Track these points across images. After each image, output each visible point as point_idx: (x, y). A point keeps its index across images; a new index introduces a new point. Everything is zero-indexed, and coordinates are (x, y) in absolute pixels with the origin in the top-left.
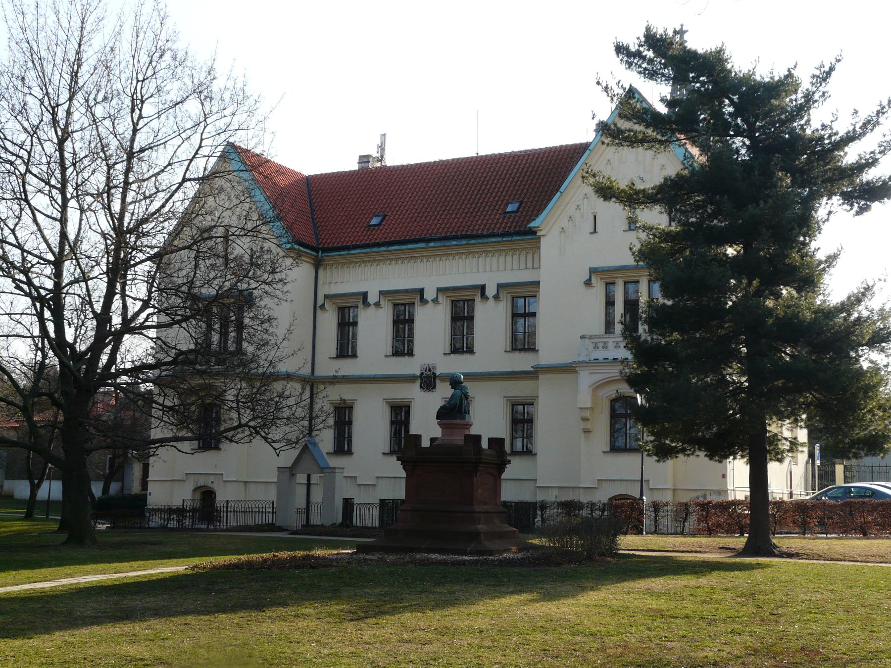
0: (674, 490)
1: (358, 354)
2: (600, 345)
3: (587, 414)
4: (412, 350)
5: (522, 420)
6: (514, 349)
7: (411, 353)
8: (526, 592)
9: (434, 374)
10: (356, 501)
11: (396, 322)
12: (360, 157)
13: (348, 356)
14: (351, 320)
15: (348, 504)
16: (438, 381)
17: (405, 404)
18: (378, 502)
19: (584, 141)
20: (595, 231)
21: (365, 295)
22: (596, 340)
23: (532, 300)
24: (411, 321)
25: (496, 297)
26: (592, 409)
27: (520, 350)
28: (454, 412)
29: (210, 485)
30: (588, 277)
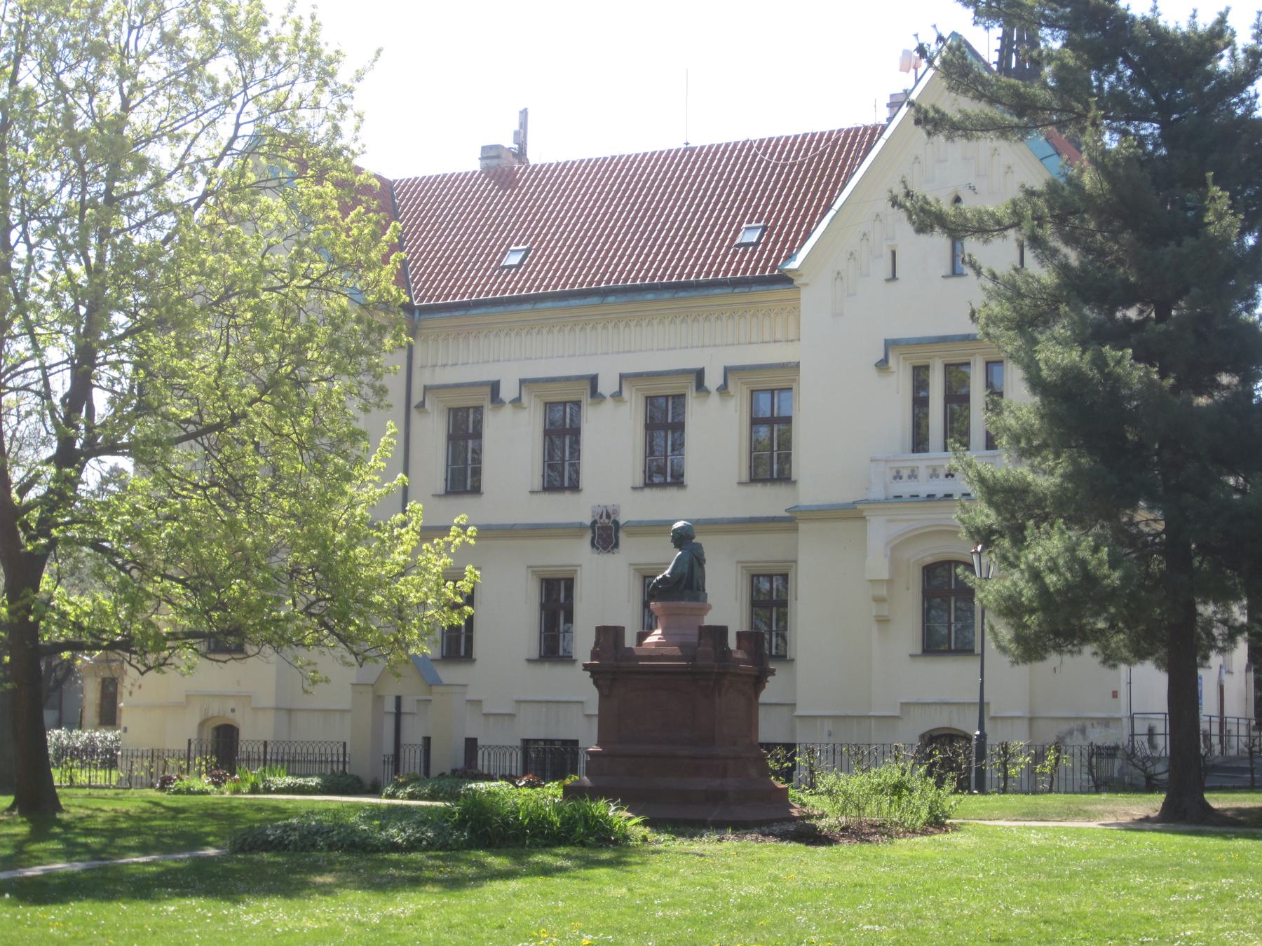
0: (1031, 719)
1: (484, 488)
2: (905, 473)
3: (883, 591)
4: (479, 487)
5: (770, 598)
6: (754, 479)
7: (575, 487)
8: (507, 855)
9: (616, 523)
10: (480, 743)
11: (652, 426)
12: (484, 148)
13: (465, 492)
14: (471, 431)
15: (471, 744)
16: (622, 535)
17: (566, 575)
18: (519, 743)
19: (870, 122)
20: (894, 277)
21: (495, 387)
22: (897, 465)
23: (784, 395)
24: (576, 432)
25: (723, 389)
26: (890, 582)
27: (764, 481)
28: (680, 588)
29: (231, 715)
30: (882, 356)
